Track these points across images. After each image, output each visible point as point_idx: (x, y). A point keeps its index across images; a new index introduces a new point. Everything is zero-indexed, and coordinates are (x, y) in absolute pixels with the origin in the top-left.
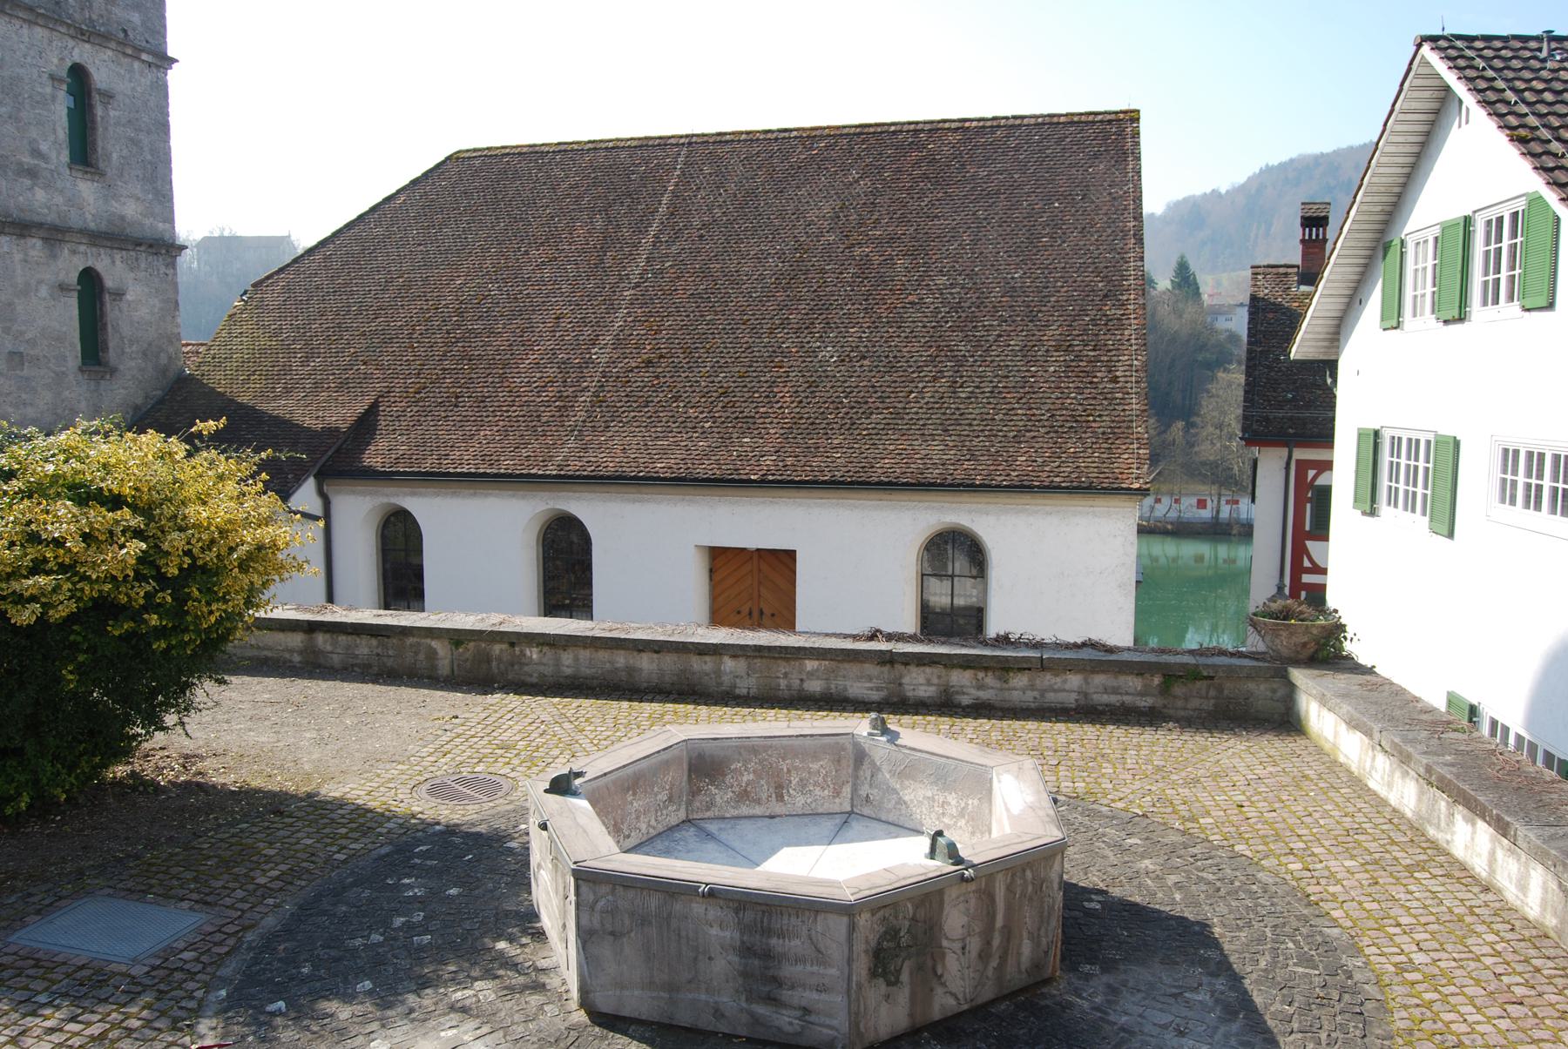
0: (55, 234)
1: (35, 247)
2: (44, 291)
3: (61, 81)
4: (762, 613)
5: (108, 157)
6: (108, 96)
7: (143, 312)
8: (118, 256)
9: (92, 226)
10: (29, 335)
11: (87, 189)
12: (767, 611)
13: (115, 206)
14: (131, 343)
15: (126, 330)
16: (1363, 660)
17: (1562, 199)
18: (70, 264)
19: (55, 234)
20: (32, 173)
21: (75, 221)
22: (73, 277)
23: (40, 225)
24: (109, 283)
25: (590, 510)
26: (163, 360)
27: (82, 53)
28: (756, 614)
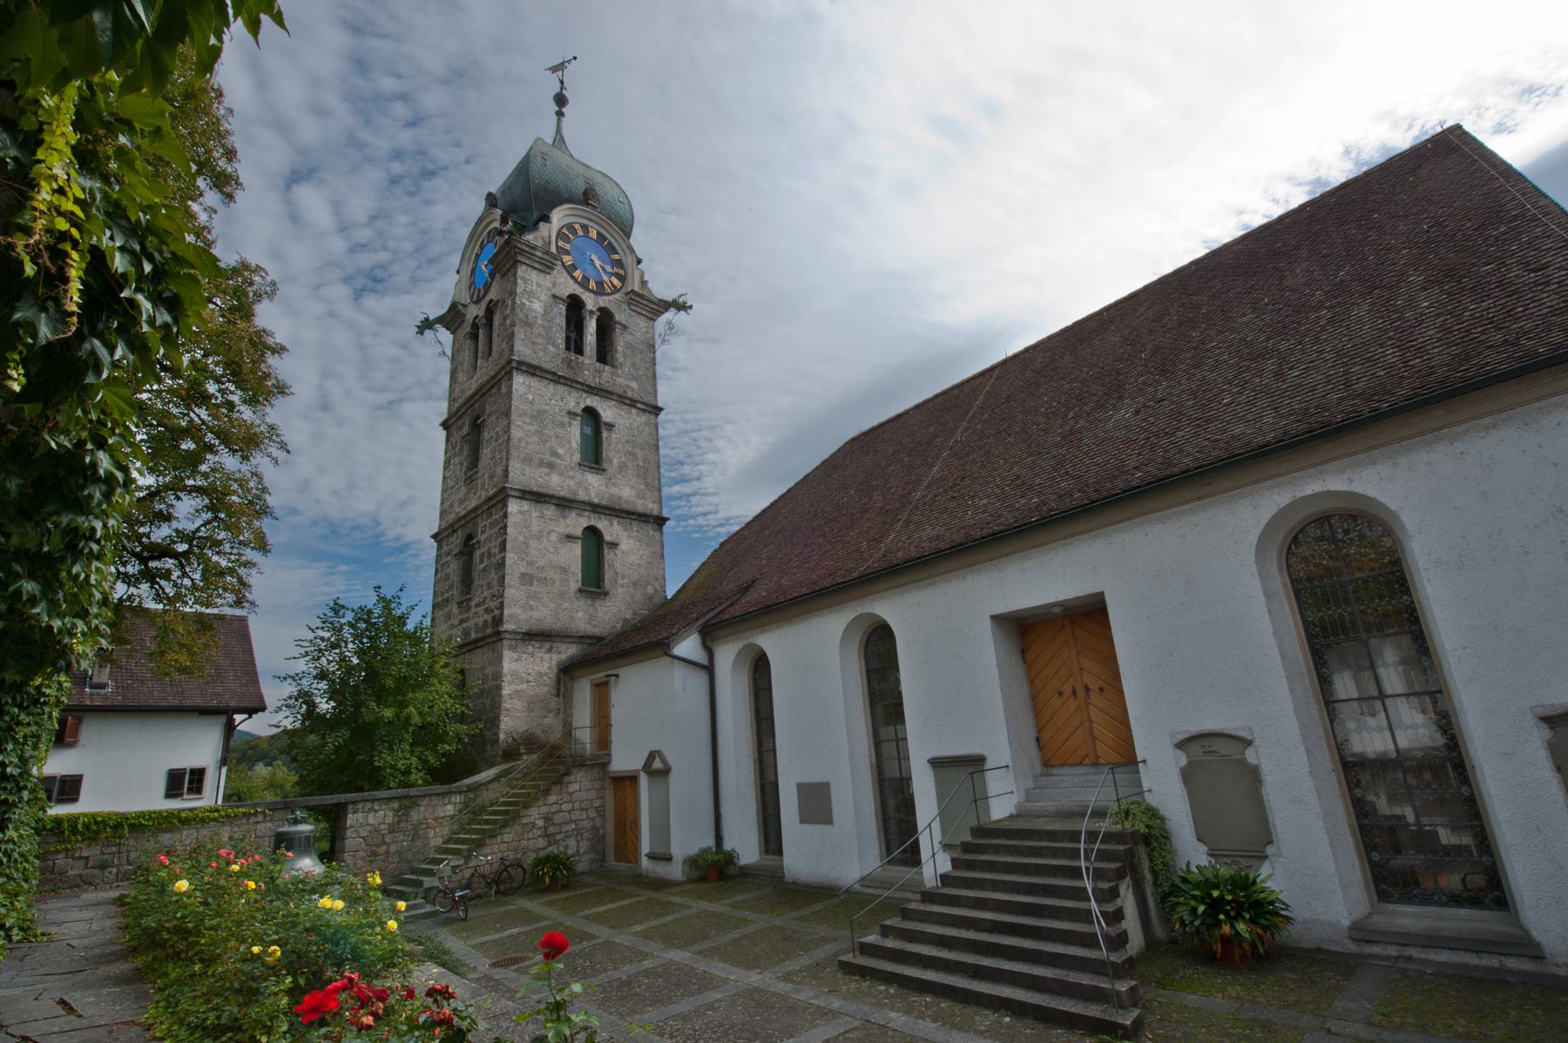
0: (565, 504)
1: (550, 511)
2: (554, 537)
3: (575, 414)
4: (1087, 689)
5: (610, 461)
6: (610, 426)
7: (633, 558)
8: (615, 522)
9: (596, 501)
10: (540, 564)
11: (593, 480)
12: (1094, 687)
13: (614, 490)
14: (623, 577)
15: (618, 568)
16: (668, 296)
17: (225, 183)
18: (577, 523)
19: (565, 504)
20: (551, 466)
21: (582, 496)
22: (578, 532)
23: (552, 497)
24: (607, 538)
25: (891, 608)
26: (650, 590)
27: (592, 401)
28: (1081, 692)
